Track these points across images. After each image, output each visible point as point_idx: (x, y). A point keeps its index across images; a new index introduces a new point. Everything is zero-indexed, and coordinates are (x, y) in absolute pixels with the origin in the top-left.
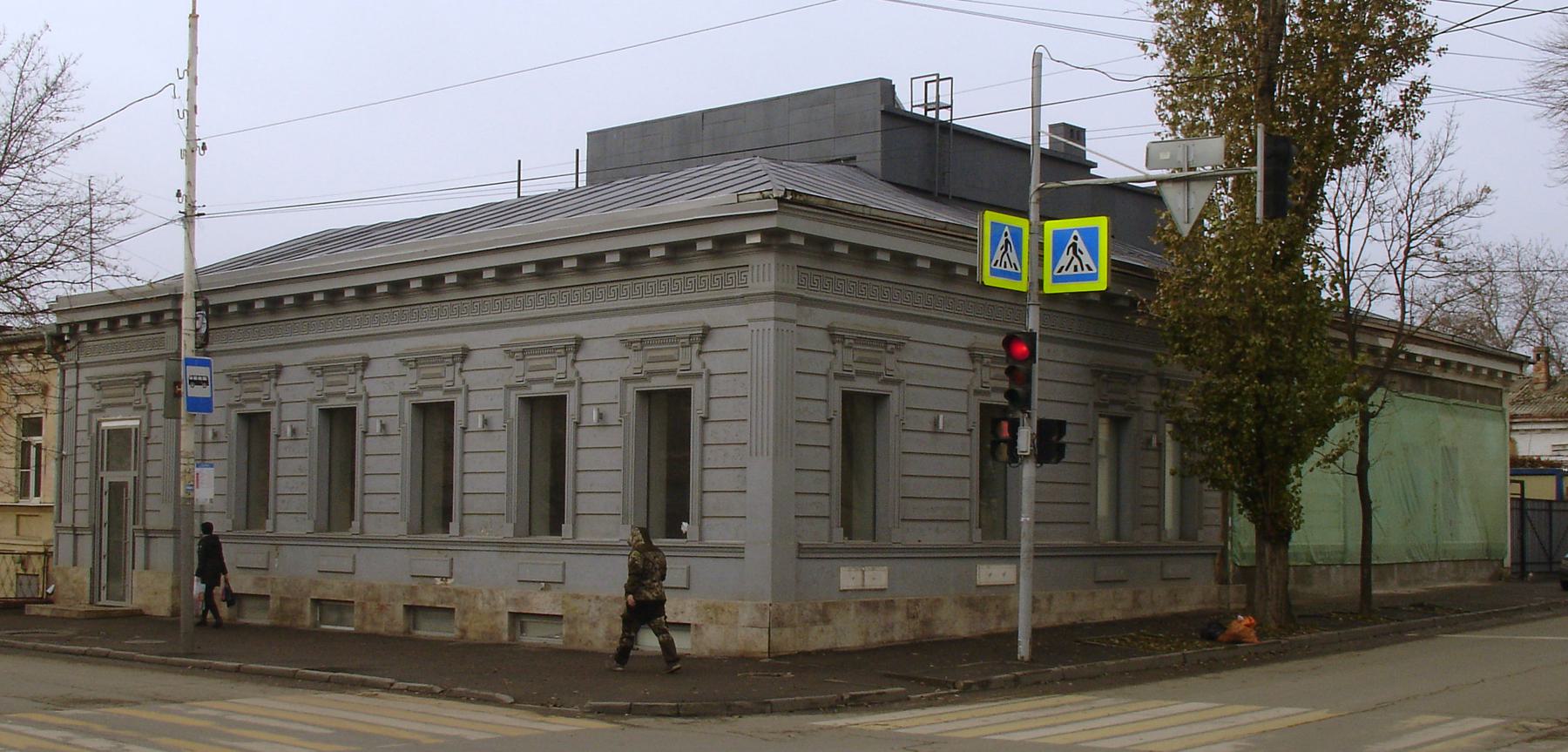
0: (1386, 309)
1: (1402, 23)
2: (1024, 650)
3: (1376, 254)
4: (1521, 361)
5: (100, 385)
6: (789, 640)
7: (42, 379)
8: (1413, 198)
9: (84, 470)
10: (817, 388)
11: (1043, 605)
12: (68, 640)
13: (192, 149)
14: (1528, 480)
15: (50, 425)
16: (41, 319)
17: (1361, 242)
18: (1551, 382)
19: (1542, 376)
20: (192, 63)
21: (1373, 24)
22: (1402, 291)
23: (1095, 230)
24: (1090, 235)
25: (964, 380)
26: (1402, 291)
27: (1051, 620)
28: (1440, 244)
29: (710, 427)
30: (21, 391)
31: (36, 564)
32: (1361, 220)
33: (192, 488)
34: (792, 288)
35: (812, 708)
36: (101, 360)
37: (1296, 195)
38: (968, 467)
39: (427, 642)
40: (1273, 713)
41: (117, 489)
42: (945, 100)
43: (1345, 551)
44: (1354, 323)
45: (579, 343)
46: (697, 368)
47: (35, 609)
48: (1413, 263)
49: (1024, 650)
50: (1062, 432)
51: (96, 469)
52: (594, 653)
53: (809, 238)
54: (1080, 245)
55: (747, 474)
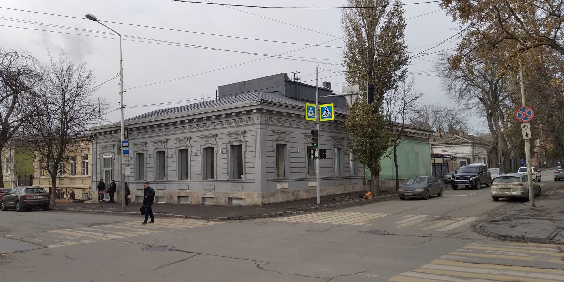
0: (400, 121)
1: (400, 57)
2: (318, 201)
3: (397, 109)
4: (433, 132)
5: (102, 148)
6: (266, 201)
7: (87, 146)
8: (405, 96)
9: (99, 168)
10: (270, 144)
11: (324, 190)
12: (94, 209)
13: (122, 92)
14: (435, 159)
15: (90, 158)
16: (88, 132)
17: (393, 107)
18: (441, 136)
19: (439, 135)
20: (121, 72)
21: (394, 57)
22: (403, 117)
23: (331, 107)
24: (330, 108)
25: (304, 141)
26: (403, 117)
27: (325, 194)
28: (411, 106)
29: (246, 153)
30: (82, 149)
31: (87, 191)
32: (393, 102)
33: (124, 172)
34: (264, 121)
35: (270, 216)
36: (102, 142)
37: (377, 96)
38: (306, 160)
39: (183, 205)
40: (375, 215)
41: (107, 172)
42: (299, 77)
43: (393, 176)
44: (392, 124)
45: (217, 135)
46: (243, 140)
47: (86, 202)
48: (405, 111)
49: (318, 201)
50: (325, 152)
51: (102, 167)
52: (221, 206)
53: (267, 110)
54: (328, 110)
55: (254, 164)
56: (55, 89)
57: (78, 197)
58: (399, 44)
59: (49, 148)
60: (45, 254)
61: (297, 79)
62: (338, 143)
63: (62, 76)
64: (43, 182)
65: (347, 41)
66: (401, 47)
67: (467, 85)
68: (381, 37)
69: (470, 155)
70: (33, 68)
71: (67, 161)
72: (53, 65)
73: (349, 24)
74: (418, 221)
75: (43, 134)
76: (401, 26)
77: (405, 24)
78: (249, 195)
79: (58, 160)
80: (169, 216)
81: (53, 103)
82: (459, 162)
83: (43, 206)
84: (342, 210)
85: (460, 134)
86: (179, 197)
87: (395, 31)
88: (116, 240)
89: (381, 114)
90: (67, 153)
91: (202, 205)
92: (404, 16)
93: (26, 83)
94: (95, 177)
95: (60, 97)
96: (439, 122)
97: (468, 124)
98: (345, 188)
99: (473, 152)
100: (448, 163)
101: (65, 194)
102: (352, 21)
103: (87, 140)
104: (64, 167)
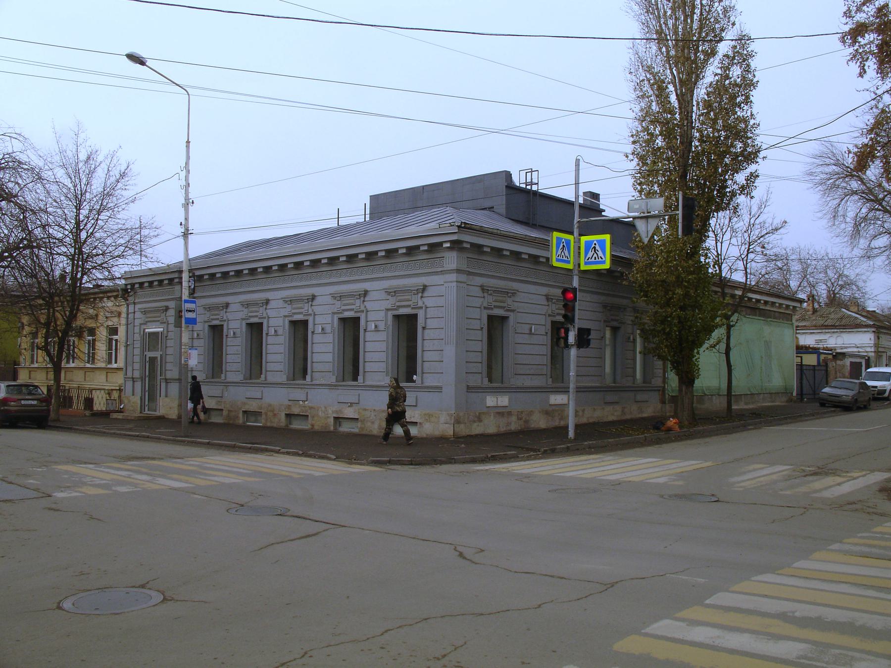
0: (738, 277)
1: (746, 145)
2: (571, 434)
3: (734, 252)
4: (801, 301)
5: (145, 312)
6: (463, 430)
7: (118, 309)
8: (751, 226)
9: (137, 351)
10: (476, 313)
11: (580, 413)
12: (130, 430)
13: (188, 203)
15: (122, 331)
17: (728, 247)
18: (815, 311)
19: (810, 308)
20: (187, 164)
21: (732, 146)
22: (746, 269)
24: (602, 243)
26: (746, 269)
27: (584, 420)
28: (763, 247)
30: (108, 315)
31: (115, 395)
32: (727, 236)
34: (464, 267)
35: (474, 461)
36: (145, 301)
37: (697, 224)
38: (546, 350)
41: (153, 360)
42: (535, 181)
43: (719, 389)
44: (724, 283)
47: (115, 416)
48: (751, 256)
49: (571, 434)
51: (143, 351)
52: (373, 436)
53: (472, 244)
54: (597, 247)
55: (444, 353)
56: (63, 198)
57: (100, 404)
58: (745, 121)
59: (48, 310)
60: (50, 509)
61: (532, 184)
62: (612, 315)
63: (77, 172)
64: (35, 372)
65: (637, 109)
66: (746, 126)
67: (870, 210)
68: (708, 105)
69: (870, 351)
70: (23, 158)
71: (80, 336)
72: (62, 152)
73: (642, 75)
74: (774, 477)
75: (39, 283)
76: (748, 84)
77: (755, 80)
78: (429, 417)
79: (66, 333)
80: (272, 451)
81: (59, 225)
82: (848, 364)
83: (37, 420)
84: (619, 452)
85: (852, 309)
86: (288, 416)
87: (733, 95)
88: (175, 489)
89: (702, 259)
90: (80, 322)
91: (335, 433)
92: (754, 63)
93: (10, 185)
94: (130, 369)
95: (71, 214)
96: (810, 284)
97: (867, 289)
98: (624, 408)
99: (876, 345)
100: (826, 365)
101: (75, 400)
102: (649, 69)
103: (116, 297)
104: (74, 347)
